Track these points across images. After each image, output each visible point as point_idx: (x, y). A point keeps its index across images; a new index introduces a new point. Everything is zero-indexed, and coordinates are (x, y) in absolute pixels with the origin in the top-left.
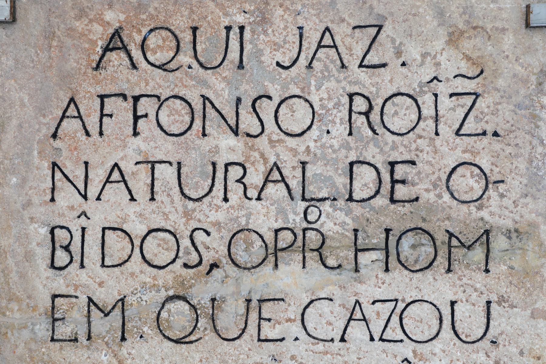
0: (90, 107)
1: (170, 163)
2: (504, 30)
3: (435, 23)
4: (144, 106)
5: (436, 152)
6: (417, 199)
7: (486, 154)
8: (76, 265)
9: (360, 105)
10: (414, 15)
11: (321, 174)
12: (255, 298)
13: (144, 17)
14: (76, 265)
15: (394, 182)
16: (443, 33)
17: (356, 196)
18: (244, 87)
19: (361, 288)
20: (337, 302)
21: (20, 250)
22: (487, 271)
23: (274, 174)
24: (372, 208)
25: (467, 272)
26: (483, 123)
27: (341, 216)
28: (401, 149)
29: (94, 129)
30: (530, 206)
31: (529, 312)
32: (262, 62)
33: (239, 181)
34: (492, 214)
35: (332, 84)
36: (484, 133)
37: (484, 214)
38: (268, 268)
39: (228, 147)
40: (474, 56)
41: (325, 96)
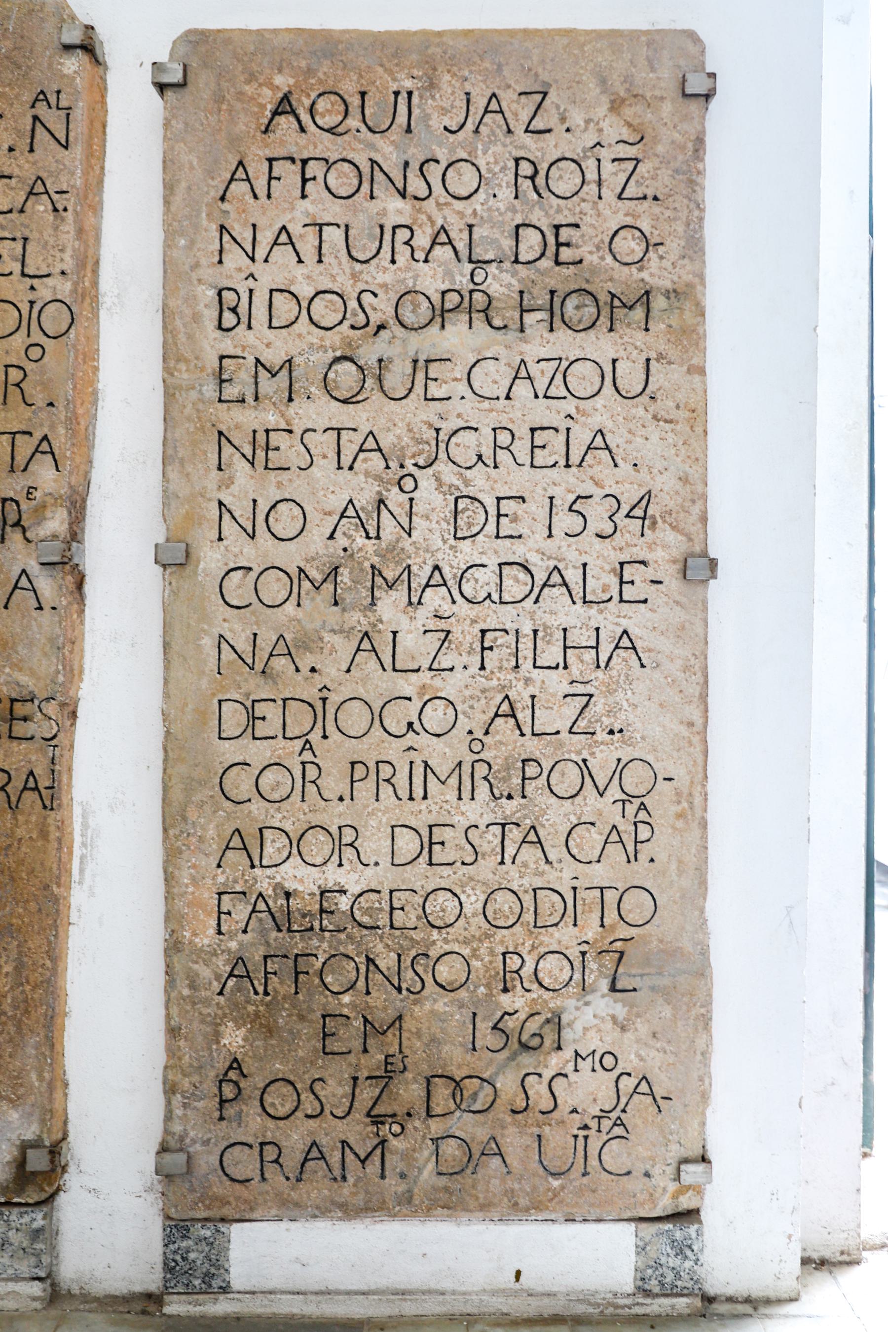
0: (258, 170)
1: (338, 226)
2: (662, 98)
3: (598, 90)
5: (599, 215)
6: (581, 261)
8: (243, 326)
9: (526, 169)
10: (578, 82)
11: (487, 237)
12: (422, 358)
13: (313, 81)
14: (243, 326)
16: (605, 100)
17: (521, 258)
18: (412, 151)
19: (526, 348)
20: (503, 361)
21: (188, 312)
22: (647, 330)
23: (441, 236)
24: (538, 270)
25: (628, 331)
28: (566, 212)
29: (262, 192)
31: (685, 368)
33: (407, 243)
34: (652, 275)
35: (499, 148)
36: (645, 198)
37: (645, 275)
38: (435, 328)
39: (395, 209)
40: (635, 122)
41: (492, 160)
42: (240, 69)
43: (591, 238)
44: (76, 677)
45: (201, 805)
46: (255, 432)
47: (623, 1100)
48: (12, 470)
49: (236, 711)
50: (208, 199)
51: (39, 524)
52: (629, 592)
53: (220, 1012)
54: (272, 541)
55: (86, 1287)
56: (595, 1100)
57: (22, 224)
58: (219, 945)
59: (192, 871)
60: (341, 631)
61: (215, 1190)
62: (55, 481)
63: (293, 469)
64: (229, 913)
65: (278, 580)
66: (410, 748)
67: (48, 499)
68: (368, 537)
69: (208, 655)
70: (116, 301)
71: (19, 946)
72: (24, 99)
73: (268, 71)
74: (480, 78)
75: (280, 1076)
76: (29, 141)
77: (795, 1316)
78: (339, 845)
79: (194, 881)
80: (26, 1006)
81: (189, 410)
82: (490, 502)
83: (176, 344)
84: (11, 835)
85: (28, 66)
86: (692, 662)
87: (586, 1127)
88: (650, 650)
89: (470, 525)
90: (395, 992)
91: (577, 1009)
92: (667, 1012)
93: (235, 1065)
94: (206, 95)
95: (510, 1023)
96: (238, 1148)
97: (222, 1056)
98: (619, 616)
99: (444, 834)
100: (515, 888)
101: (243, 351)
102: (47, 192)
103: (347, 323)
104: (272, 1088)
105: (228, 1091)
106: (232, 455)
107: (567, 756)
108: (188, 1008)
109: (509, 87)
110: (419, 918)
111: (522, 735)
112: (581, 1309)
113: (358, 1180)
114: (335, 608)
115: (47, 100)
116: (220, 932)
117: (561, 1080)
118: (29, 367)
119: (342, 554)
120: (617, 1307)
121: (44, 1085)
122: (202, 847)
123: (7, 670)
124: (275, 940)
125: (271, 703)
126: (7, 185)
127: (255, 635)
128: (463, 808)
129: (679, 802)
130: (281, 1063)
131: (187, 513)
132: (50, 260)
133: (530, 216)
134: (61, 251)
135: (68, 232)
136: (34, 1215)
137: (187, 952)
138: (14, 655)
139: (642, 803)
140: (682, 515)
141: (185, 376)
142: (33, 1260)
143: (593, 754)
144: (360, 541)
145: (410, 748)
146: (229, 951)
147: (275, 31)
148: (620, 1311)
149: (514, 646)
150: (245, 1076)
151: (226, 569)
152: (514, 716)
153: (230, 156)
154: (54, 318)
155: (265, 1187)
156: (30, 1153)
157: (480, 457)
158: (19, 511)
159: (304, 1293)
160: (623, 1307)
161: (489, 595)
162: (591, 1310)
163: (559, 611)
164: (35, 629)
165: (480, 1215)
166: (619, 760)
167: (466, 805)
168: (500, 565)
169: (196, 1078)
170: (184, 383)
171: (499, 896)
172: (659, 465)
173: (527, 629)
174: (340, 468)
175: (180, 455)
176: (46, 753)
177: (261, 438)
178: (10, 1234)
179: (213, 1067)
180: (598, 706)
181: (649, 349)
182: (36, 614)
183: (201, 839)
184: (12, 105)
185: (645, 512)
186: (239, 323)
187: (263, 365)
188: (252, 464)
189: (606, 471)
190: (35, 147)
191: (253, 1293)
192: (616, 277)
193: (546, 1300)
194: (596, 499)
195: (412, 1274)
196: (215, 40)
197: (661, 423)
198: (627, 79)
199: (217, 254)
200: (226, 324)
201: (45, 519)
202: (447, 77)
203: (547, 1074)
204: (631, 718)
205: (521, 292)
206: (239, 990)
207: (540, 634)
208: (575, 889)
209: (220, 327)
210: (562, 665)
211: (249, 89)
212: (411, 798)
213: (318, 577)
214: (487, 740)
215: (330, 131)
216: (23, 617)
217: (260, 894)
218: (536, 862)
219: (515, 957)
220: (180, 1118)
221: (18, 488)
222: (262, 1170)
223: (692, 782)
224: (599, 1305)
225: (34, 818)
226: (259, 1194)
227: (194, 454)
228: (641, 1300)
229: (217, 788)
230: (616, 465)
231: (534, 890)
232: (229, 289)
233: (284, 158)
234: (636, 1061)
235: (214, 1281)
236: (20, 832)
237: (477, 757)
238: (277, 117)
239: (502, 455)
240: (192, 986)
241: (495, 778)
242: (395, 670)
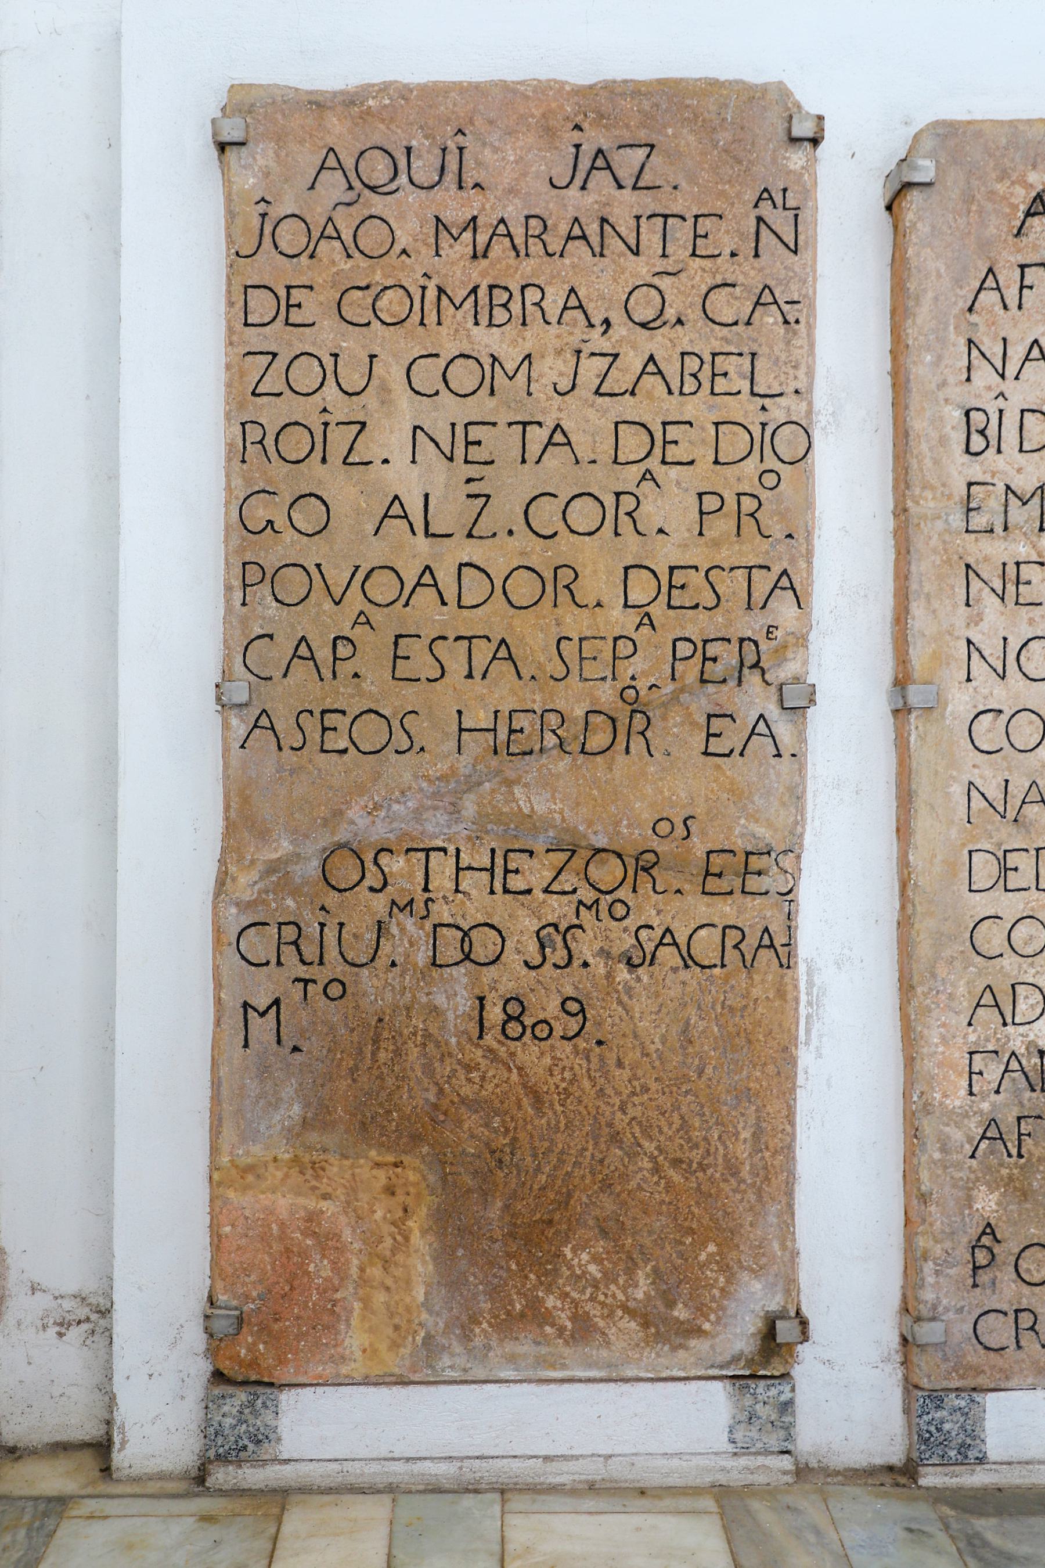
0: (1009, 278)
8: (992, 450)
14: (992, 450)
21: (934, 435)
42: (992, 165)
45: (951, 961)
46: (1004, 564)
48: (749, 608)
49: (987, 862)
50: (956, 310)
51: (779, 665)
53: (972, 1176)
54: (1023, 682)
55: (825, 1460)
57: (749, 338)
58: (971, 1107)
59: (942, 1030)
61: (969, 1358)
62: (798, 619)
64: (981, 1073)
65: (1031, 723)
67: (790, 639)
69: (957, 803)
70: (831, 420)
71: (757, 1110)
72: (747, 197)
73: (1022, 167)
75: (1036, 1241)
76: (753, 245)
79: (944, 1040)
80: (766, 1174)
81: (934, 541)
83: (921, 470)
84: (746, 996)
85: (749, 161)
93: (988, 1230)
96: (993, 1315)
97: (975, 1221)
101: (993, 477)
102: (776, 302)
104: (1027, 1253)
105: (982, 1258)
106: (980, 590)
108: (939, 1172)
115: (771, 198)
116: (971, 1094)
118: (764, 495)
121: (787, 1254)
122: (953, 1004)
123: (743, 821)
124: (1030, 1100)
125: (1024, 853)
126: (731, 294)
127: (1007, 781)
130: (1036, 1227)
131: (934, 652)
132: (783, 378)
134: (795, 367)
135: (801, 347)
136: (781, 1388)
137: (938, 1114)
138: (750, 806)
141: (931, 504)
142: (782, 1434)
146: (981, 1112)
147: (1029, 121)
150: (998, 1242)
151: (976, 712)
153: (980, 263)
154: (789, 442)
155: (1021, 1355)
156: (780, 1325)
158: (758, 652)
164: (773, 777)
169: (948, 1245)
170: (929, 513)
175: (926, 590)
176: (782, 908)
177: (1011, 570)
178: (758, 1407)
179: (965, 1232)
182: (774, 761)
183: (951, 997)
184: (733, 204)
186: (987, 447)
187: (1013, 492)
188: (1003, 599)
190: (761, 252)
191: (1010, 1463)
196: (964, 132)
199: (965, 370)
200: (974, 448)
201: (786, 660)
206: (992, 1153)
209: (967, 451)
211: (1001, 188)
216: (761, 765)
217: (1013, 1053)
220: (932, 1286)
221: (757, 627)
222: (1017, 1337)
225: (770, 977)
226: (1016, 1362)
227: (941, 589)
229: (968, 943)
232: (978, 410)
233: (1036, 265)
235: (969, 1451)
236: (755, 992)
238: (1029, 219)
240: (944, 1150)
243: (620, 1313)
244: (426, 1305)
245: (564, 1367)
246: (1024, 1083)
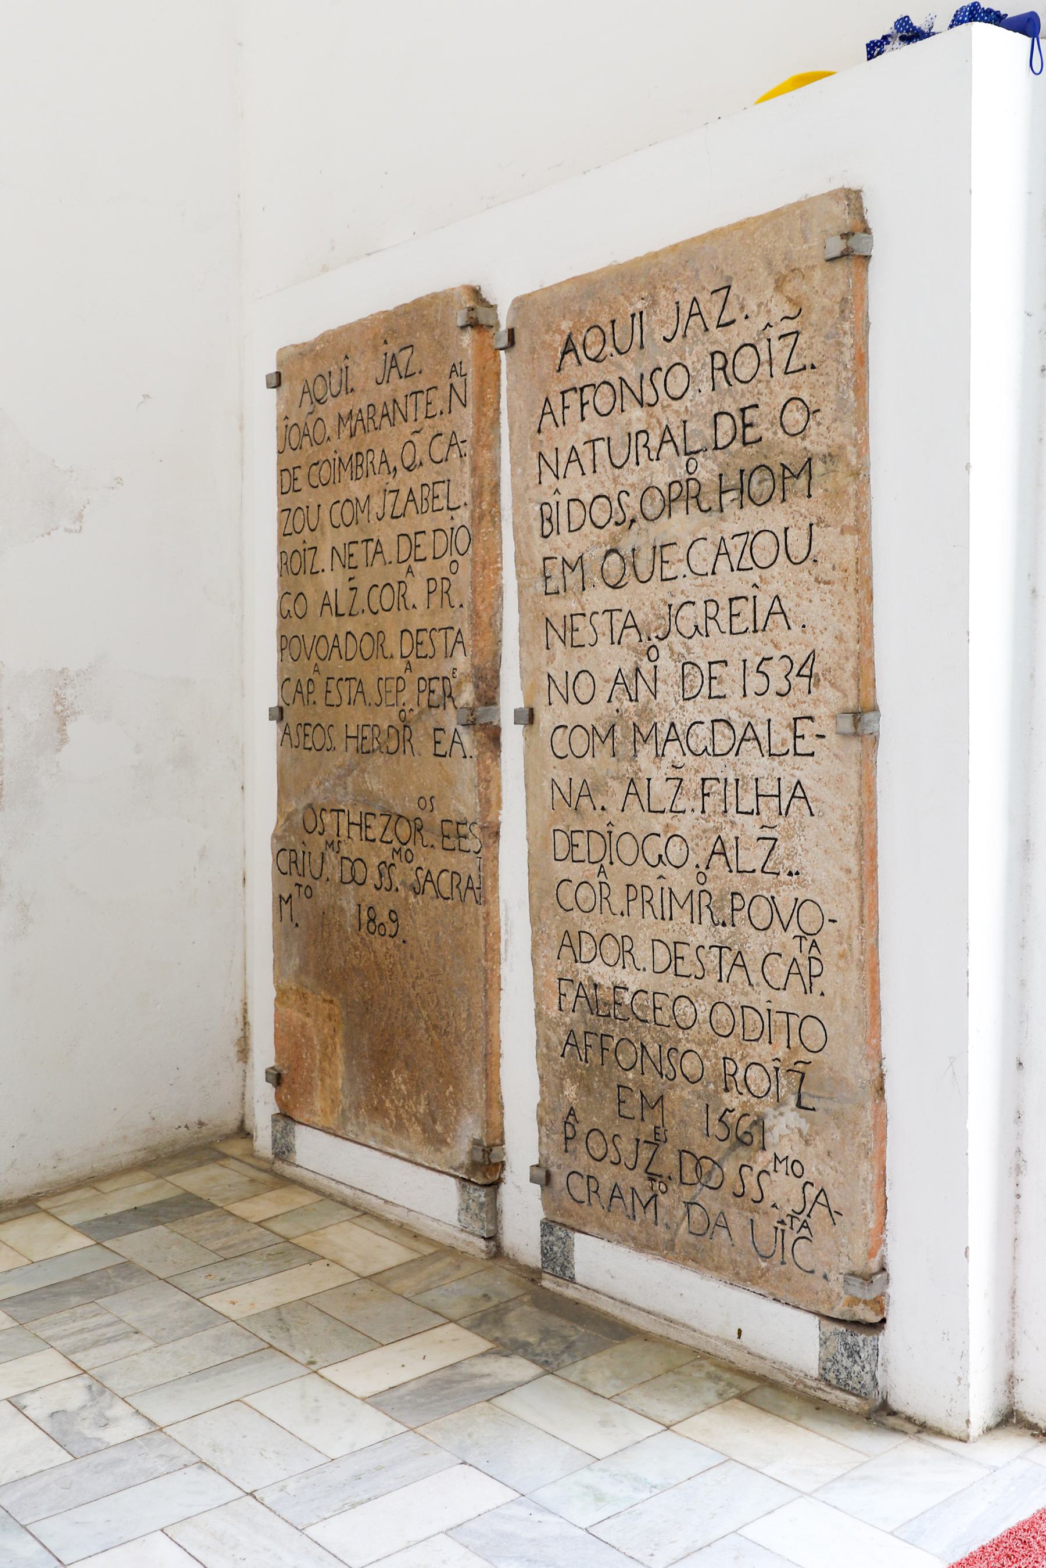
0: (556, 402)
1: (603, 439)
2: (814, 267)
3: (766, 274)
4: (588, 393)
5: (771, 393)
6: (760, 439)
7: (806, 386)
8: (555, 532)
9: (719, 361)
10: (751, 270)
11: (695, 430)
12: (658, 544)
13: (583, 320)
14: (555, 532)
15: (745, 426)
16: (771, 281)
17: (719, 446)
18: (645, 364)
19: (724, 525)
20: (709, 540)
21: (525, 526)
22: (809, 496)
23: (667, 437)
24: (730, 454)
25: (795, 499)
26: (803, 359)
27: (709, 463)
28: (748, 395)
29: (560, 421)
30: (839, 430)
31: (839, 529)
32: (654, 340)
33: (645, 446)
34: (812, 442)
35: (698, 348)
36: (804, 368)
37: (806, 443)
38: (664, 518)
39: (636, 416)
40: (794, 297)
41: (695, 359)
43: (766, 415)
44: (494, 807)
47: (809, 1206)
52: (802, 746)
56: (788, 1200)
60: (618, 778)
63: (587, 645)
65: (582, 736)
66: (661, 877)
68: (631, 700)
74: (685, 286)
77: (941, 1448)
78: (623, 952)
82: (704, 666)
86: (849, 812)
87: (782, 1222)
88: (817, 800)
89: (692, 687)
90: (658, 1076)
91: (775, 1117)
92: (838, 1135)
94: (525, 349)
95: (730, 1118)
98: (794, 768)
99: (682, 950)
100: (730, 1004)
103: (612, 521)
107: (760, 893)
109: (704, 288)
110: (670, 1017)
111: (731, 871)
112: (780, 1378)
113: (642, 1220)
114: (613, 759)
116: (560, 1009)
117: (763, 1176)
118: (452, 578)
119: (616, 714)
120: (806, 1386)
128: (695, 931)
129: (841, 943)
133: (724, 405)
139: (814, 941)
140: (838, 672)
143: (778, 892)
144: (627, 703)
145: (661, 877)
147: (559, 285)
148: (807, 1390)
149: (723, 793)
152: (725, 854)
155: (590, 1210)
157: (697, 627)
159: (615, 1299)
160: (811, 1388)
161: (706, 749)
162: (787, 1381)
163: (754, 763)
165: (715, 1274)
166: (797, 899)
167: (696, 928)
168: (713, 721)
171: (719, 1007)
172: (820, 626)
173: (731, 780)
174: (613, 643)
180: (780, 850)
181: (811, 514)
183: (549, 937)
185: (811, 671)
189: (782, 634)
192: (786, 449)
193: (757, 1361)
194: (775, 660)
195: (676, 1309)
197: (822, 585)
198: (787, 256)
200: (546, 533)
202: (663, 292)
203: (757, 1169)
204: (804, 862)
205: (721, 475)
207: (740, 783)
208: (769, 1010)
210: (755, 811)
212: (663, 918)
213: (603, 732)
214: (708, 873)
215: (594, 360)
218: (742, 983)
219: (732, 1063)
223: (850, 926)
224: (793, 1379)
228: (823, 1387)
230: (789, 628)
231: (742, 1007)
234: (816, 1173)
237: (702, 888)
239: (711, 624)
241: (714, 907)
242: (650, 811)
243: (414, 1119)
244: (342, 1090)
245: (393, 1147)
246: (587, 1008)
